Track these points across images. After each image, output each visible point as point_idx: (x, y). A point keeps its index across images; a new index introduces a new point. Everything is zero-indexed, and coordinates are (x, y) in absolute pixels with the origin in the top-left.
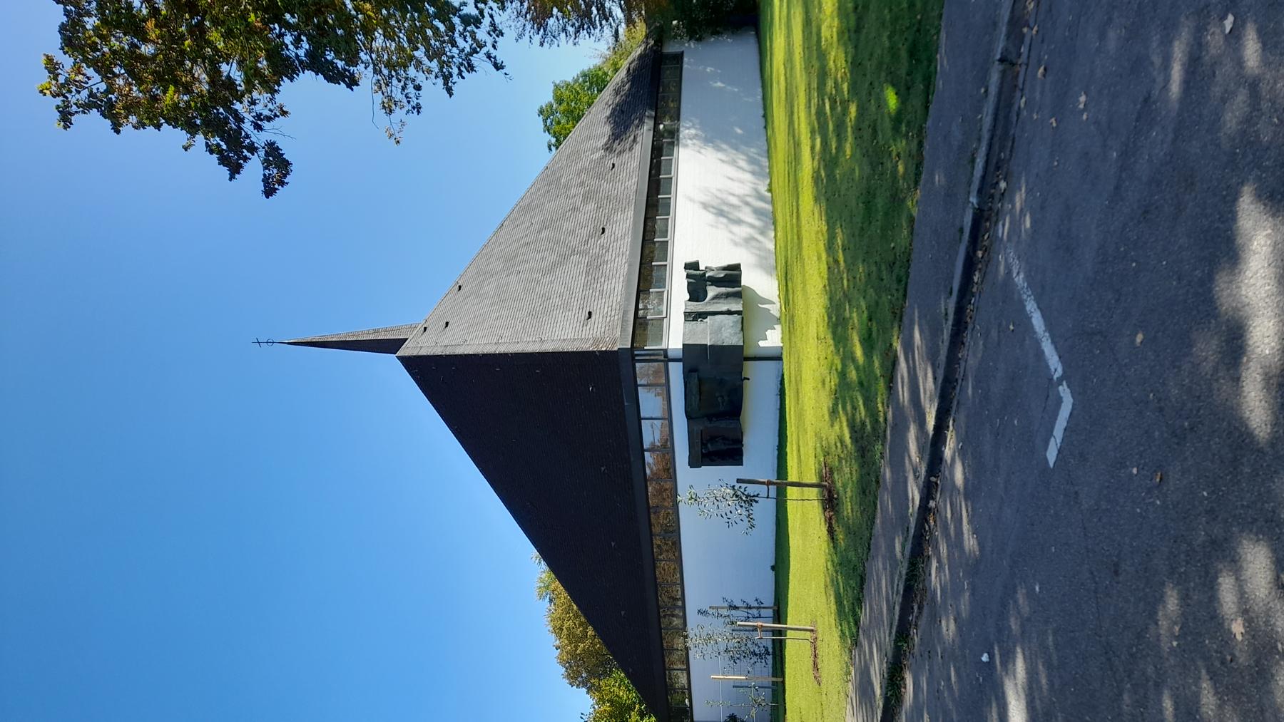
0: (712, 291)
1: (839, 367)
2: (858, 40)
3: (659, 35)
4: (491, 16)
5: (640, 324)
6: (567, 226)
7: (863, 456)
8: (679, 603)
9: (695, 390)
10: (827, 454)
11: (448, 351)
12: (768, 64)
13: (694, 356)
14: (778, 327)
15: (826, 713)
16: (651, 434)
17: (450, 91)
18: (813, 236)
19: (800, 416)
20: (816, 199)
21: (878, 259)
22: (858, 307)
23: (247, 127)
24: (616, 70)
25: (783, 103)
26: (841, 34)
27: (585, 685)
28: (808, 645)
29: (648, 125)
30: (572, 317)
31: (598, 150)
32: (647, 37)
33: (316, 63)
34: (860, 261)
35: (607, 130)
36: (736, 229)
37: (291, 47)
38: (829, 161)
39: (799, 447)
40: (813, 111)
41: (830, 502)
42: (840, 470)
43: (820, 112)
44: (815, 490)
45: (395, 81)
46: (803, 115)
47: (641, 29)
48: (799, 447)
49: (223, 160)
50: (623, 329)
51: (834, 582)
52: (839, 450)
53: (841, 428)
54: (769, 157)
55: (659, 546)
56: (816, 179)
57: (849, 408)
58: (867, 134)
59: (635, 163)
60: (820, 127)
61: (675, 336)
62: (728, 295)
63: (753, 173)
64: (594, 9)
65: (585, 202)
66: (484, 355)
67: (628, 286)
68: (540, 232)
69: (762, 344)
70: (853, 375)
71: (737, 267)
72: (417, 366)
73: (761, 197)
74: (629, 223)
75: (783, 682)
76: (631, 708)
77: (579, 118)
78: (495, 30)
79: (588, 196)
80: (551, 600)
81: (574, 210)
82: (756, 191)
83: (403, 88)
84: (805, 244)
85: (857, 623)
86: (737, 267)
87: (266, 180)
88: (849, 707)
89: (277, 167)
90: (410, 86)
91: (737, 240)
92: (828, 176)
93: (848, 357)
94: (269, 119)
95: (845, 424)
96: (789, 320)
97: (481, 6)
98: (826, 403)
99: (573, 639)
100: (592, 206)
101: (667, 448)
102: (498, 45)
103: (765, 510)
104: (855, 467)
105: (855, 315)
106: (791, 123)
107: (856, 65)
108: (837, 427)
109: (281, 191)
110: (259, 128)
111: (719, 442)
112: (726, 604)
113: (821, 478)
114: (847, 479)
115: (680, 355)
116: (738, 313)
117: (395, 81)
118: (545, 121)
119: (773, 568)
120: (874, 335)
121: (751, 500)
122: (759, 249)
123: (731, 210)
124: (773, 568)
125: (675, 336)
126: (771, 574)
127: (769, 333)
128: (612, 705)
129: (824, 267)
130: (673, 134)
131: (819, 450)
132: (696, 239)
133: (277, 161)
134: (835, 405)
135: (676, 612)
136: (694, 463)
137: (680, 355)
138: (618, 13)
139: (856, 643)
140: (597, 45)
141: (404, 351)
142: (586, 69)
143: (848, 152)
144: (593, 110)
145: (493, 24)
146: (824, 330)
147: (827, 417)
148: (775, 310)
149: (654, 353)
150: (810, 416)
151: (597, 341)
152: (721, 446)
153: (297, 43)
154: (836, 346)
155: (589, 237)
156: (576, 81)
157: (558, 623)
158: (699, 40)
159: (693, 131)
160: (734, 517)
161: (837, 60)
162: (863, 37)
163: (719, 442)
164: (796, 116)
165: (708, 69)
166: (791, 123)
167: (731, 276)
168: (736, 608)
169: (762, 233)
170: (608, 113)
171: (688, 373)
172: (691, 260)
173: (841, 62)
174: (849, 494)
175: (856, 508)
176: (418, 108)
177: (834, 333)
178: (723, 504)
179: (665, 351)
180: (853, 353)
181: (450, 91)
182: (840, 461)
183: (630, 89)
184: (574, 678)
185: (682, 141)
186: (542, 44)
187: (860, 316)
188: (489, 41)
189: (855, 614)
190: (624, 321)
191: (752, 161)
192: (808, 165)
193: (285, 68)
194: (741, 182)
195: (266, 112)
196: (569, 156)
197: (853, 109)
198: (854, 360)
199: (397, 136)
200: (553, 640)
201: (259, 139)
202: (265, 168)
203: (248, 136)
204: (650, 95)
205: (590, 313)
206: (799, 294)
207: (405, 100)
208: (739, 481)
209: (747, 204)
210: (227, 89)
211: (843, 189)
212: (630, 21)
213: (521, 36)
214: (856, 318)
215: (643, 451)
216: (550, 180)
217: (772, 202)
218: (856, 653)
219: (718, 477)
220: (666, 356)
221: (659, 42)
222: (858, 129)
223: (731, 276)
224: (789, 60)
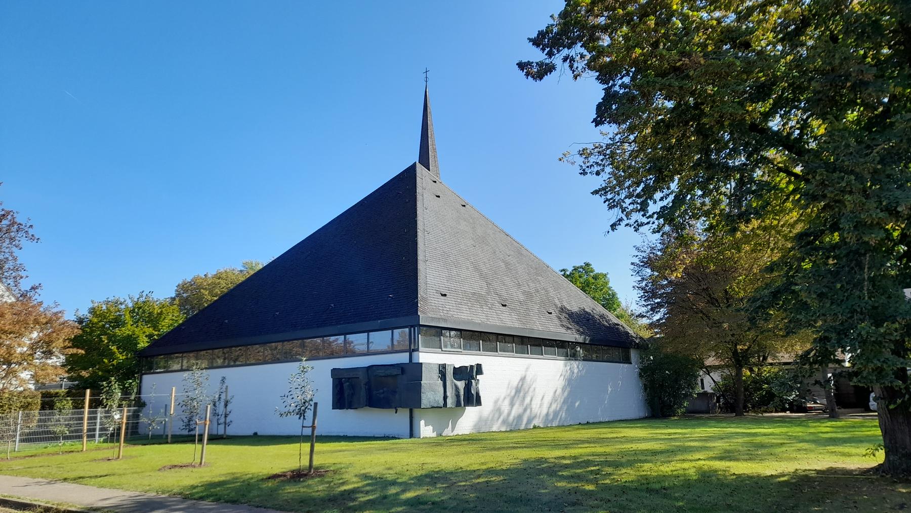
0: (461, 384)
1: (399, 481)
2: (641, 490)
3: (643, 346)
4: (648, 223)
5: (439, 331)
6: (507, 280)
7: (330, 500)
8: (233, 362)
9: (388, 372)
10: (335, 472)
11: (419, 197)
12: (624, 425)
13: (414, 371)
14: (434, 435)
15: (135, 475)
16: (358, 340)
17: (595, 192)
18: (500, 459)
19: (367, 452)
20: (525, 461)
21: (479, 508)
22: (444, 494)
23: (565, 52)
24: (618, 317)
25: (597, 436)
26: (646, 478)
27: (177, 295)
28: (190, 461)
29: (580, 339)
30: (444, 282)
31: (561, 302)
32: (641, 338)
33: (610, 96)
34: (478, 495)
35: (575, 309)
36: (507, 402)
37: (620, 82)
38: (553, 470)
39: (344, 451)
40: (590, 458)
41: (298, 476)
42: (322, 483)
43: (588, 463)
44: (308, 464)
45: (602, 157)
46: (588, 450)
47: (646, 334)
48: (344, 451)
49: (542, 34)
50: (433, 319)
51: (235, 480)
52: (336, 482)
53: (354, 483)
54: (558, 427)
55: (276, 348)
56: (540, 461)
57: (368, 488)
58: (573, 498)
59: (552, 329)
60: (578, 463)
61: (429, 358)
62: (458, 396)
63: (547, 415)
64: (659, 300)
65: (524, 293)
66: (416, 222)
67: (464, 322)
68: (503, 261)
69: (422, 423)
70: (393, 490)
71: (478, 402)
72: (409, 176)
73: (529, 421)
74: (509, 324)
75: (167, 443)
76: (155, 327)
77: (585, 291)
78: (638, 226)
79: (528, 295)
80: (241, 271)
81: (519, 285)
82: (535, 417)
83: (597, 163)
84: (495, 453)
85: (201, 498)
86: (478, 402)
87: (529, 64)
88: (137, 493)
89: (538, 71)
90: (599, 168)
91: (499, 402)
92: (543, 469)
93: (406, 487)
94: (571, 67)
95: (356, 485)
96: (440, 442)
97: (655, 216)
98: (373, 471)
99: (214, 285)
100: (522, 298)
101: (348, 352)
102: (628, 227)
103: (293, 425)
104: (322, 494)
105: (438, 491)
106: (583, 442)
107: (624, 489)
108: (355, 479)
109: (522, 74)
110: (565, 60)
111: (349, 391)
112: (229, 398)
113: (317, 469)
114: (316, 488)
115: (414, 361)
116: (445, 404)
117: (602, 157)
118: (581, 267)
119: (256, 434)
120: (422, 507)
121: (301, 414)
122: (492, 420)
123: (520, 398)
124: (256, 434)
125: (429, 358)
126: (251, 433)
127: (430, 428)
128: (158, 314)
129: (476, 467)
130: (574, 356)
131: (339, 466)
132: (499, 373)
133: (544, 70)
134: (372, 478)
135: (227, 361)
136: (334, 371)
137: (414, 361)
138: (657, 317)
139: (186, 498)
140: (634, 303)
141: (420, 169)
142: (618, 296)
143: (559, 484)
144: (589, 300)
145: (642, 224)
146: (429, 468)
147: (363, 472)
148: (448, 432)
149: (416, 342)
150: (368, 458)
151: (425, 300)
152: (347, 393)
153: (623, 86)
154: (416, 477)
155: (500, 296)
156: (610, 288)
157: (224, 276)
158: (640, 376)
159: (576, 371)
160: (289, 401)
161: (627, 475)
162: (644, 494)
163: (349, 391)
164: (587, 445)
165: (620, 381)
166: (583, 442)
167: (472, 398)
168: (226, 405)
169: (504, 422)
170: (587, 310)
171: (401, 367)
172: (484, 368)
173: (625, 478)
174: (302, 490)
175: (290, 496)
176: (584, 173)
177: (426, 476)
178: (298, 392)
179: (417, 350)
180: (409, 490)
181: (595, 192)
182: (329, 482)
183: (604, 325)
184: (184, 287)
185: (569, 363)
186: (632, 264)
187: (436, 495)
188: (631, 222)
189: (208, 497)
190: (439, 319)
191: (556, 414)
192: (551, 454)
193: (606, 74)
195: (575, 65)
196: (556, 282)
197: (590, 487)
198: (404, 491)
199: (565, 159)
200: (212, 272)
201: (557, 60)
202: (537, 63)
203: (559, 51)
204: (600, 340)
205: (445, 295)
206: (459, 449)
207: (589, 164)
208: (316, 404)
209: (525, 410)
210: (591, 37)
211: (533, 481)
212: (651, 326)
213: (638, 249)
214: (435, 492)
215: (345, 334)
216: (540, 269)
217: (526, 429)
218: (179, 498)
219: (324, 392)
220: (414, 350)
221: (638, 347)
222: (576, 491)
223: (472, 398)
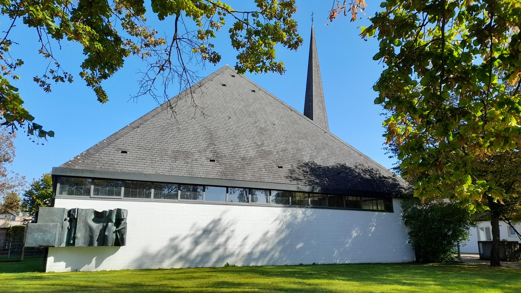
62: (91, 237)
63: (250, 254)
73: (221, 259)
91: (176, 242)
194: (242, 245)
224: (295, 283)
